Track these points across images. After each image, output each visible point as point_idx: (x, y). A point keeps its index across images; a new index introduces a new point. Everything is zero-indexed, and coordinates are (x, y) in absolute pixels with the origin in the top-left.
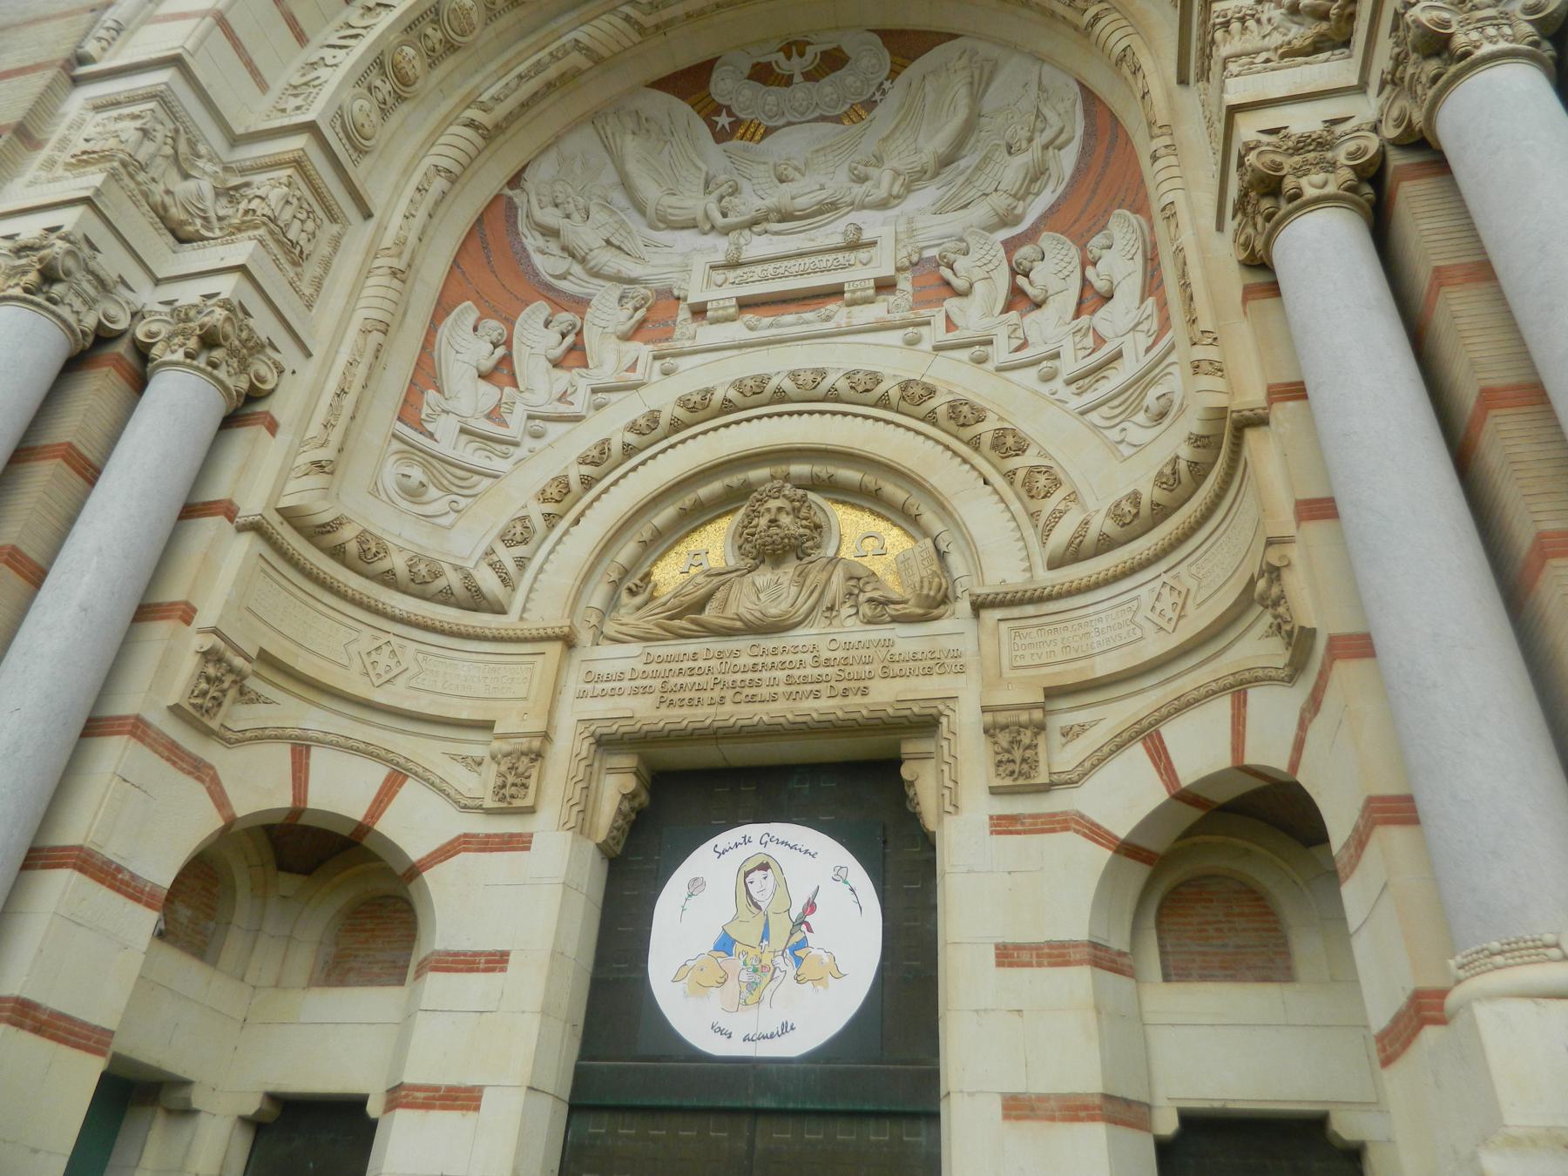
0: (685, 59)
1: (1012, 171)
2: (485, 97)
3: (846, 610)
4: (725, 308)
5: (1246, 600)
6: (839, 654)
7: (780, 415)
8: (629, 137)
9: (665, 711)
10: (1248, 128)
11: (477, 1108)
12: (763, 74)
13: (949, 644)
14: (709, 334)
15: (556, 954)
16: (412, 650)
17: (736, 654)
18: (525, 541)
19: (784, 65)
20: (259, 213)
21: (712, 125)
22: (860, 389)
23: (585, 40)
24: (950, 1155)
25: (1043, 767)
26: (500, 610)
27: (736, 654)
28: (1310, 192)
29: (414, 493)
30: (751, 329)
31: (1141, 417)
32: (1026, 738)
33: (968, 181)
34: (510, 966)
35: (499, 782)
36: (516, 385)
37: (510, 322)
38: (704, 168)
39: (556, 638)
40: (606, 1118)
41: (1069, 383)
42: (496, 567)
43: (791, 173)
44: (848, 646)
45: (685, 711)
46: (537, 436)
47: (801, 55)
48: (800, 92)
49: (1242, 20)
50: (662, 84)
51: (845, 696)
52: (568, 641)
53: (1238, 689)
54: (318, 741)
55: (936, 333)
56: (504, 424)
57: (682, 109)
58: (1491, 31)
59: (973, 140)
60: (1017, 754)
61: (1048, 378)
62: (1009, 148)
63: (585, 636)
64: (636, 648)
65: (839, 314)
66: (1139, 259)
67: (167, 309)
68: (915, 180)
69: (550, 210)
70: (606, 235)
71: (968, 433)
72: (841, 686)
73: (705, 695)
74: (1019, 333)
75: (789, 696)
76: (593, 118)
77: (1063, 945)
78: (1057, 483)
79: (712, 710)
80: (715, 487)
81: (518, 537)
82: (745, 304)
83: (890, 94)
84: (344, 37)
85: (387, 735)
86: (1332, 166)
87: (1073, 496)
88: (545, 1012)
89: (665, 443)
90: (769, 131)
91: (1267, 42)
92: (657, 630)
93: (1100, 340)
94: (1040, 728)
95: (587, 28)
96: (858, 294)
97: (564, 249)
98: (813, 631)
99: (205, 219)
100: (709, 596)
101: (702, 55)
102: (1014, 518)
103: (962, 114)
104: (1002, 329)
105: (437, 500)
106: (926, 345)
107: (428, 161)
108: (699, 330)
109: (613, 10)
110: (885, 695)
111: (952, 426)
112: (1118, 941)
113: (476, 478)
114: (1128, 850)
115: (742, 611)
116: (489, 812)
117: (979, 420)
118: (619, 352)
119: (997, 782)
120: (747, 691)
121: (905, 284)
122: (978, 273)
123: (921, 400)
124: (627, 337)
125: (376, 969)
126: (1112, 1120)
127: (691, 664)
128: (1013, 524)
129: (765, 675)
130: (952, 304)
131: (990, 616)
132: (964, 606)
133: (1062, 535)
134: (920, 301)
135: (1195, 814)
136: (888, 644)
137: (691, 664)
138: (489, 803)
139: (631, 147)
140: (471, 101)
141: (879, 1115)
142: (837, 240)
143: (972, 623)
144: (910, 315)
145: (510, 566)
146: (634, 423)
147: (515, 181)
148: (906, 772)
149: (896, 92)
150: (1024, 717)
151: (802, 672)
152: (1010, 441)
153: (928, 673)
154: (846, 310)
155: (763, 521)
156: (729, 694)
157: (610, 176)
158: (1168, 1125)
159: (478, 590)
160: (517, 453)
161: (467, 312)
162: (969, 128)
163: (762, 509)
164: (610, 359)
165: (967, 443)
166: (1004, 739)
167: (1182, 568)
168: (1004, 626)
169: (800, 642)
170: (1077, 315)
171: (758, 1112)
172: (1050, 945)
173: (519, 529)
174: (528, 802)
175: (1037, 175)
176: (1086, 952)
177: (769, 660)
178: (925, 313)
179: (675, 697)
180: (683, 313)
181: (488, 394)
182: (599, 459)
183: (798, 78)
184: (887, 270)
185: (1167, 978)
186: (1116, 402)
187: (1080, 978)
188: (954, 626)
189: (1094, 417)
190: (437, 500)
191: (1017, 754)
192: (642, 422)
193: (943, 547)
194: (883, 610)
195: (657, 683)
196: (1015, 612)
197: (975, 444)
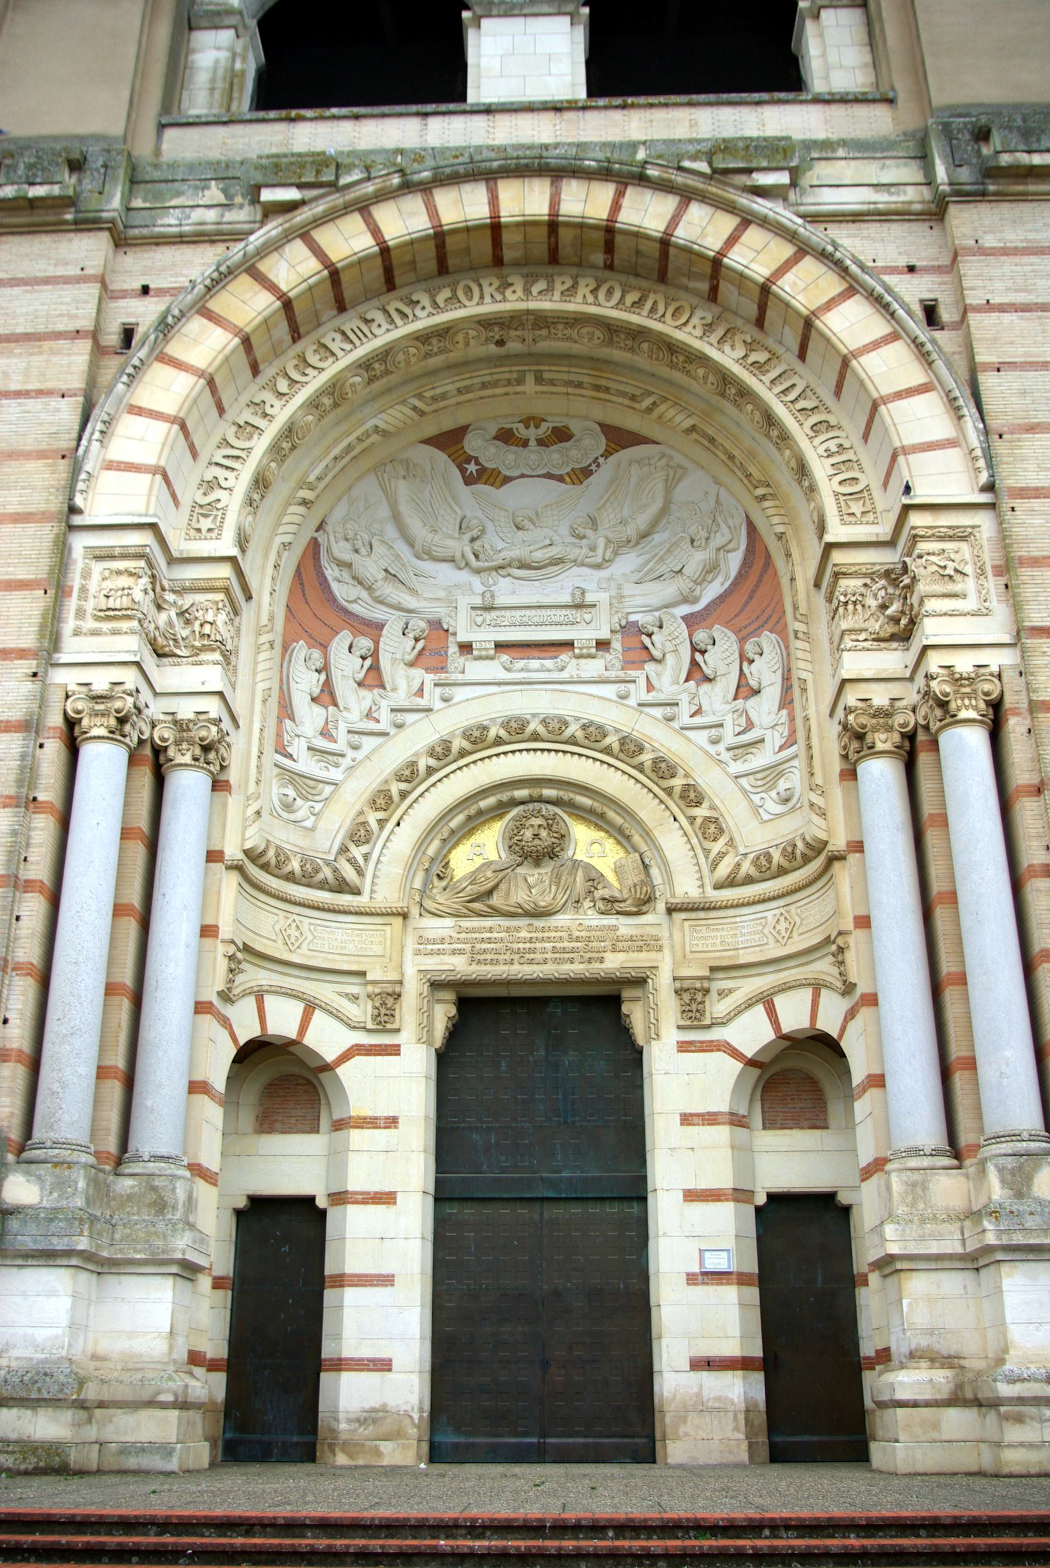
0: (447, 423)
1: (695, 560)
2: (312, 478)
3: (587, 904)
4: (486, 649)
5: (827, 941)
6: (584, 934)
7: (535, 750)
8: (401, 482)
9: (474, 967)
10: (851, 698)
11: (395, 1203)
12: (506, 436)
13: (652, 931)
14: (477, 670)
15: (427, 1117)
16: (308, 922)
17: (518, 929)
18: (367, 842)
19: (522, 431)
20: (213, 638)
21: (463, 471)
22: (592, 739)
23: (382, 425)
24: (657, 1220)
25: (708, 1015)
26: (357, 892)
27: (518, 929)
28: (880, 746)
29: (288, 807)
30: (507, 670)
31: (773, 794)
32: (699, 997)
33: (662, 559)
34: (401, 1125)
35: (376, 1012)
36: (336, 705)
37: (324, 647)
38: (459, 512)
39: (399, 914)
40: (456, 1204)
41: (729, 749)
42: (352, 861)
43: (527, 524)
44: (590, 929)
45: (488, 968)
46: (355, 748)
47: (537, 427)
48: (533, 454)
49: (855, 603)
50: (428, 441)
51: (589, 962)
52: (405, 916)
53: (817, 987)
54: (268, 991)
55: (638, 693)
56: (333, 740)
57: (441, 458)
58: (967, 702)
59: (664, 521)
60: (694, 1007)
61: (715, 742)
62: (692, 541)
63: (415, 911)
64: (449, 922)
65: (573, 667)
66: (779, 673)
67: (169, 718)
68: (619, 547)
69: (343, 544)
70: (385, 565)
71: (665, 784)
72: (587, 956)
73: (501, 957)
74: (696, 701)
75: (555, 961)
76: (377, 468)
77: (715, 1114)
78: (721, 831)
79: (506, 968)
80: (490, 801)
81: (363, 839)
82: (500, 646)
83: (603, 468)
84: (228, 457)
85: (299, 982)
86: (890, 729)
87: (731, 842)
88: (425, 1151)
89: (454, 766)
90: (507, 480)
91: (866, 625)
92: (465, 911)
93: (750, 725)
94: (707, 991)
95: (383, 416)
96: (585, 651)
97: (354, 578)
98: (567, 917)
99: (175, 640)
100: (496, 887)
101: (461, 422)
102: (693, 849)
103: (658, 504)
104: (684, 692)
105: (303, 809)
106: (632, 702)
107: (278, 540)
108: (467, 664)
109: (404, 402)
110: (614, 963)
111: (654, 776)
112: (743, 1111)
113: (321, 785)
114: (751, 1063)
115: (520, 901)
116: (369, 1031)
117: (673, 776)
118: (407, 677)
119: (682, 1023)
120: (527, 956)
121: (617, 645)
122: (669, 647)
123: (634, 755)
124: (411, 664)
125: (293, 1121)
126: (736, 1200)
127: (489, 935)
128: (692, 853)
129: (538, 945)
130: (650, 667)
131: (678, 916)
132: (661, 907)
133: (724, 869)
134: (628, 664)
135: (787, 1043)
136: (615, 928)
137: (489, 935)
138: (370, 1026)
139: (403, 489)
140: (303, 484)
141: (611, 1199)
142: (566, 598)
143: (666, 917)
144: (621, 674)
145: (361, 860)
146: (433, 749)
147: (320, 527)
148: (625, 1008)
149: (608, 467)
150: (698, 985)
151: (561, 945)
152: (692, 795)
153: (640, 950)
154: (574, 661)
155: (528, 834)
156: (516, 957)
157: (383, 511)
158: (761, 1200)
159: (344, 880)
160: (346, 762)
161: (301, 649)
162: (664, 511)
163: (528, 824)
164: (402, 685)
165: (664, 790)
166: (686, 997)
167: (792, 908)
168: (687, 923)
169: (560, 924)
170: (735, 698)
171: (543, 1199)
172: (709, 1113)
173: (363, 832)
174: (395, 1026)
175: (711, 569)
176: (727, 1118)
177: (540, 935)
178: (633, 673)
179: (482, 957)
180: (453, 649)
181: (368, 697)
182: (409, 774)
183: (533, 443)
184: (604, 634)
185: (764, 1128)
186: (759, 776)
187: (722, 1133)
188: (654, 918)
189: (744, 781)
190: (303, 809)
191: (694, 1007)
192: (438, 749)
193: (647, 861)
194: (611, 905)
195: (468, 947)
196: (693, 915)
197: (669, 791)
